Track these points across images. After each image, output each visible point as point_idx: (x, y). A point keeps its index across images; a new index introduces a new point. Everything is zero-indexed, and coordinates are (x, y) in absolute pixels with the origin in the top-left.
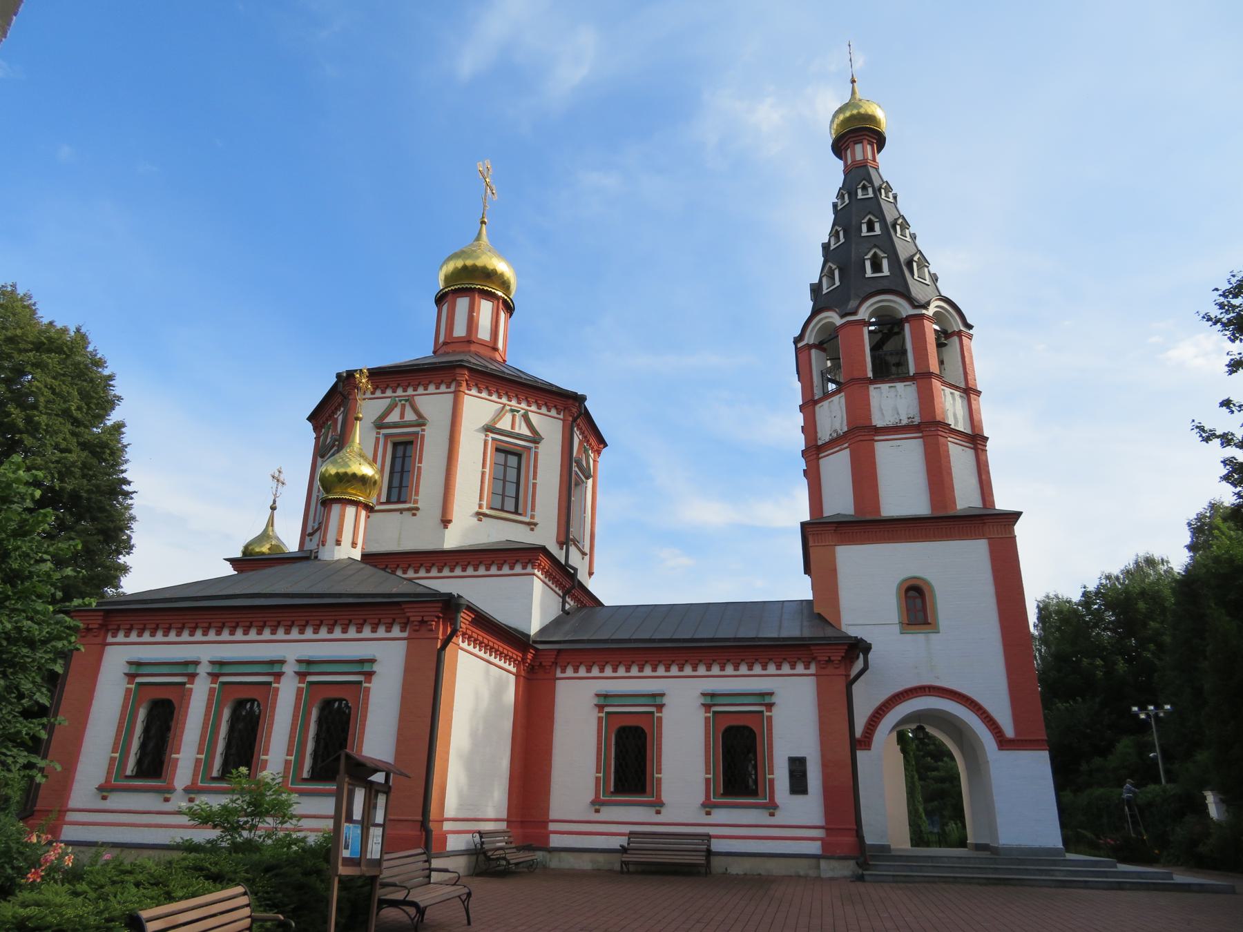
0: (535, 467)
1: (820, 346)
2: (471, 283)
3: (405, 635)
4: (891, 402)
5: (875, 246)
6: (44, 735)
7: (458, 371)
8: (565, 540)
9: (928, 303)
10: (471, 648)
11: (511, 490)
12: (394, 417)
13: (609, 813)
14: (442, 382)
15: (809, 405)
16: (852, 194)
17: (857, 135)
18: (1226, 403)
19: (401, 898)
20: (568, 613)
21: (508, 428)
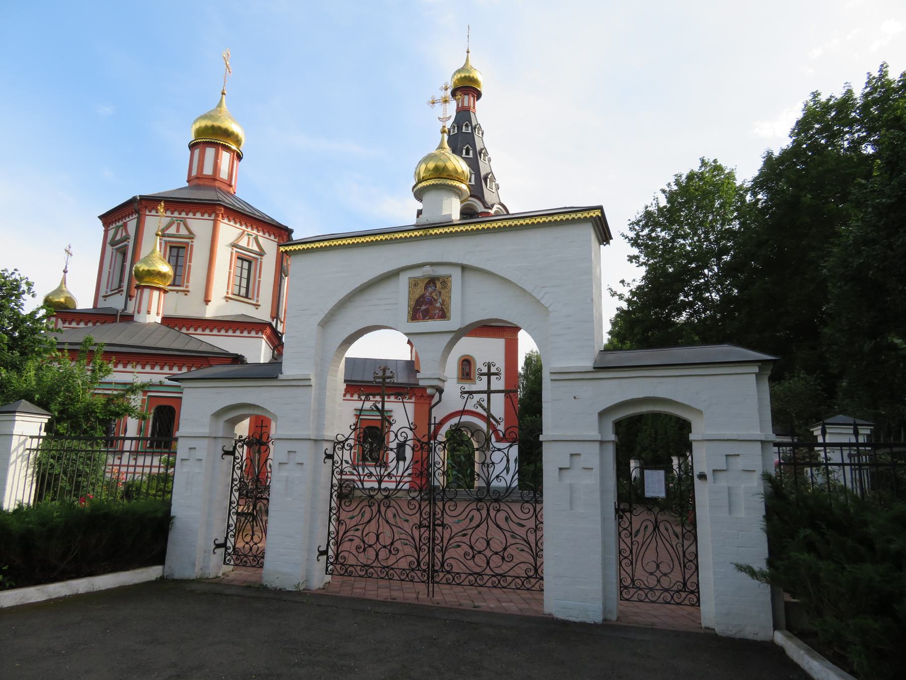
2: (212, 138)
7: (218, 207)
8: (276, 315)
9: (493, 206)
11: (244, 283)
12: (172, 230)
16: (460, 128)
17: (466, 88)
18: (622, 282)
21: (245, 245)
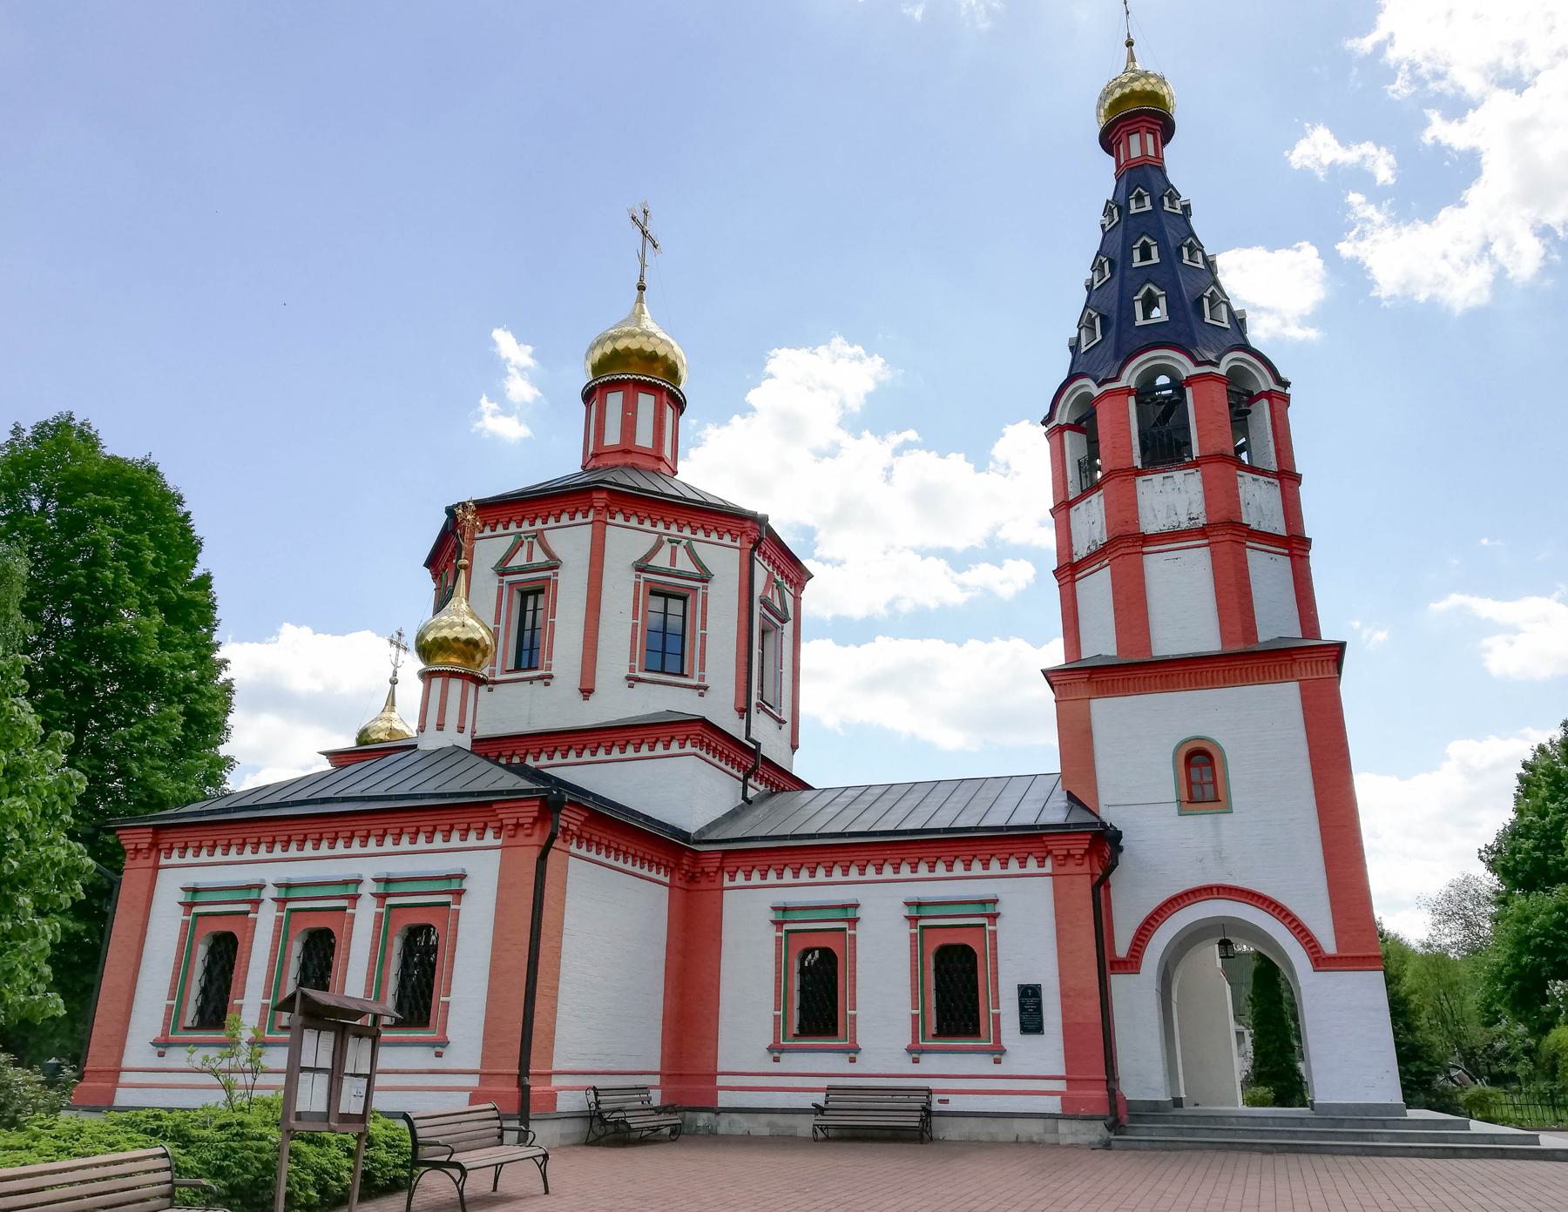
0: (704, 613)
1: (1075, 427)
3: (499, 842)
4: (1170, 498)
5: (1148, 281)
10: (583, 852)
12: (519, 560)
13: (791, 1062)
14: (563, 511)
15: (1063, 507)
17: (1137, 119)
19: (444, 1158)
20: (749, 802)
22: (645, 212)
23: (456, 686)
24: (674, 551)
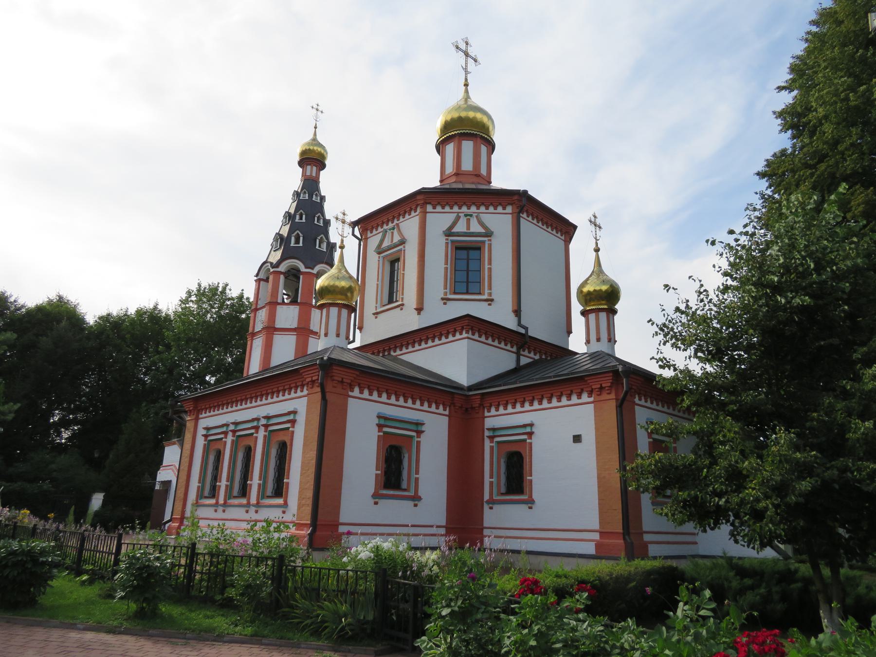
3: (591, 399)
6: (652, 518)
22: (467, 43)
23: (334, 311)
24: (468, 221)
